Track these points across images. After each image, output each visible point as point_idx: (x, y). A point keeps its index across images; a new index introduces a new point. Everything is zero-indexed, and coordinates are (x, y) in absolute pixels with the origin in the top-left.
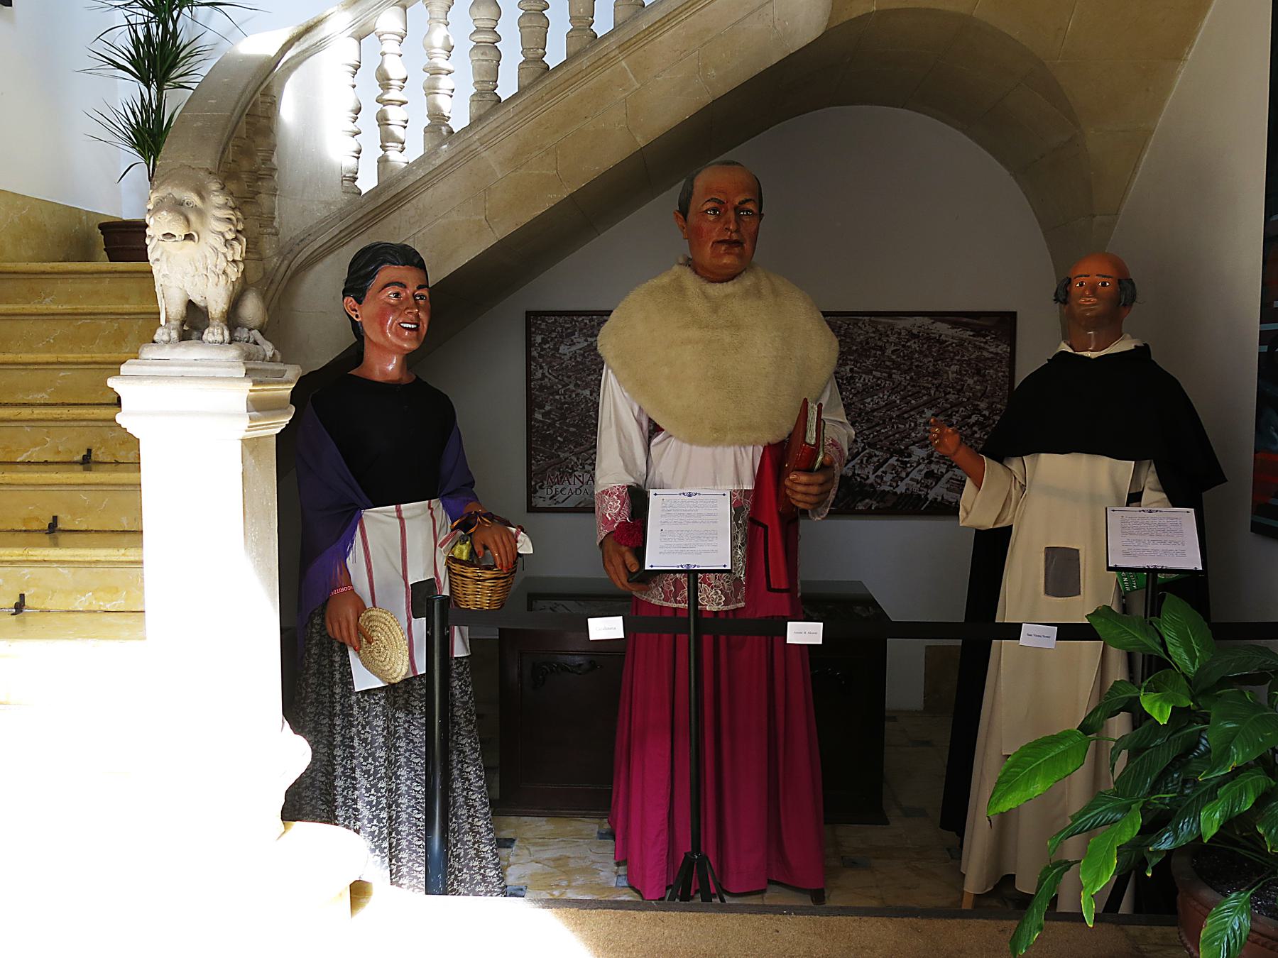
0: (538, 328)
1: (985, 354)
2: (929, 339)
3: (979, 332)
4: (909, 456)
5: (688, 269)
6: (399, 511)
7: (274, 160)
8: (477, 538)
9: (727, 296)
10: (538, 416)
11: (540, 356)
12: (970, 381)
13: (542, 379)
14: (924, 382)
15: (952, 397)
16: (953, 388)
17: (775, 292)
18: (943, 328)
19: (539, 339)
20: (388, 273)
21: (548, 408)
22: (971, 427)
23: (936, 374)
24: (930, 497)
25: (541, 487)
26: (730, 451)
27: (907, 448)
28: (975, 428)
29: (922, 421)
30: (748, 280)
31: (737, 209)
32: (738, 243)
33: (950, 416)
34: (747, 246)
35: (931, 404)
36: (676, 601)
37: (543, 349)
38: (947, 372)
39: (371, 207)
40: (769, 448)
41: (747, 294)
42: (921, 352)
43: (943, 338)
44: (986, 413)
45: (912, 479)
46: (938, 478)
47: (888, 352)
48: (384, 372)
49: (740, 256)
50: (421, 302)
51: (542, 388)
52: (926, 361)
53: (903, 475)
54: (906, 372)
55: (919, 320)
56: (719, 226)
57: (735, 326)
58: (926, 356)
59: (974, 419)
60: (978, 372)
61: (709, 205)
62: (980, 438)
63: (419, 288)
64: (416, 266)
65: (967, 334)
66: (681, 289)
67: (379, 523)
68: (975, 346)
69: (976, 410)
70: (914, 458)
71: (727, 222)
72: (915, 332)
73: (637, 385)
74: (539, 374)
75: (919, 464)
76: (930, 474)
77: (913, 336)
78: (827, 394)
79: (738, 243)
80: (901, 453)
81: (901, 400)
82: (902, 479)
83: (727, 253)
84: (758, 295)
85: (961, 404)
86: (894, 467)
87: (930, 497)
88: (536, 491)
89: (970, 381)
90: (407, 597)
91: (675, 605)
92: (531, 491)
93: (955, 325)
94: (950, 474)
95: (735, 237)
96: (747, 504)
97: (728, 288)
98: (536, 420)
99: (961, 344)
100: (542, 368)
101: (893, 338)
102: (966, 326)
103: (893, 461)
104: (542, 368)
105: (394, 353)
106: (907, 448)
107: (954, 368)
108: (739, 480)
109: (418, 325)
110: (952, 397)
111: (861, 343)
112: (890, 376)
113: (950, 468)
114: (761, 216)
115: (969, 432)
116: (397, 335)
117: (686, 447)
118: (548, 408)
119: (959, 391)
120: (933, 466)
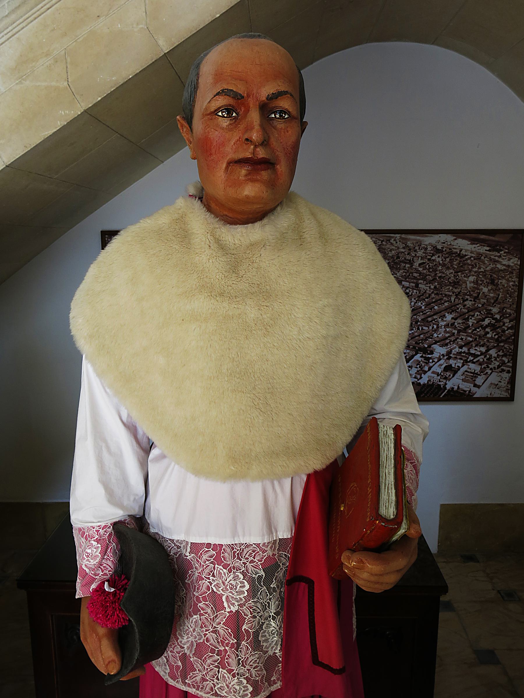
1: (499, 266)
2: (451, 253)
3: (494, 247)
4: (432, 353)
5: (197, 204)
9: (252, 245)
12: (485, 290)
14: (445, 290)
15: (469, 304)
16: (470, 295)
17: (323, 237)
18: (463, 244)
22: (484, 328)
23: (456, 284)
24: (448, 387)
26: (256, 489)
27: (429, 346)
28: (488, 330)
29: (443, 323)
30: (284, 220)
31: (265, 108)
32: (267, 164)
33: (467, 319)
34: (282, 168)
35: (451, 309)
36: (185, 683)
38: (465, 282)
40: (315, 480)
41: (281, 242)
42: (444, 265)
43: (463, 252)
44: (498, 316)
45: (433, 372)
46: (455, 371)
47: (416, 264)
49: (271, 184)
52: (448, 272)
53: (426, 368)
54: (431, 282)
55: (443, 237)
56: (235, 136)
57: (263, 293)
58: (448, 268)
59: (487, 321)
60: (492, 282)
61: (221, 101)
62: (492, 338)
65: (483, 249)
66: (184, 236)
68: (491, 259)
69: (489, 314)
70: (436, 355)
71: (249, 128)
72: (439, 247)
73: (124, 382)
75: (439, 359)
76: (448, 368)
77: (437, 251)
78: (395, 377)
79: (267, 164)
80: (425, 351)
81: (426, 306)
82: (425, 372)
83: (250, 178)
84: (300, 241)
85: (476, 309)
86: (418, 363)
87: (448, 387)
89: (485, 290)
91: (184, 688)
93: (473, 241)
94: (465, 368)
95: (261, 153)
96: (284, 563)
97: (254, 232)
99: (479, 257)
101: (420, 253)
102: (482, 242)
103: (418, 357)
106: (429, 346)
107: (472, 279)
108: (270, 525)
110: (469, 304)
111: (392, 257)
112: (417, 285)
113: (466, 362)
114: (303, 126)
115: (482, 333)
117: (192, 479)
119: (476, 298)
120: (452, 362)
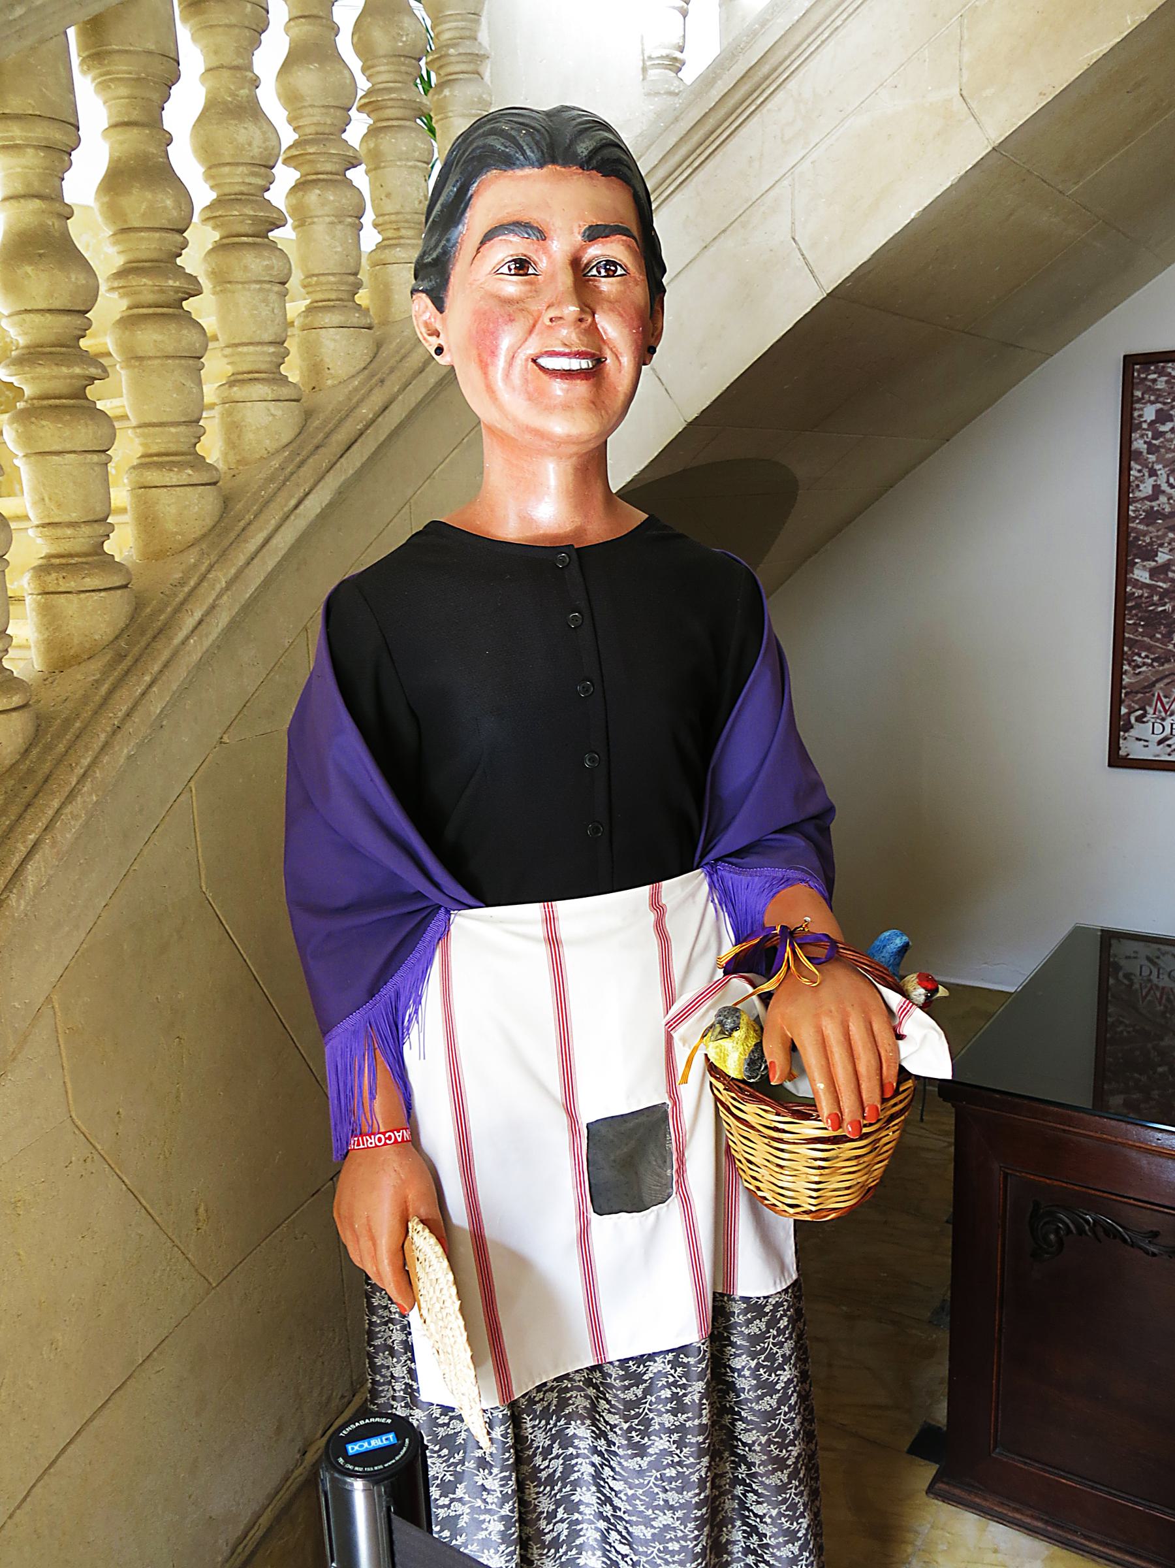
0: (1150, 390)
6: (550, 920)
7: (483, 36)
8: (779, 1016)
10: (1141, 574)
11: (1152, 449)
13: (1154, 497)
19: (1149, 413)
20: (497, 196)
21: (1162, 557)
25: (1139, 719)
37: (1158, 435)
39: (695, 114)
48: (526, 520)
50: (607, 285)
51: (1152, 516)
63: (594, 234)
64: (586, 164)
67: (489, 954)
74: (1146, 489)
88: (1128, 727)
90: (576, 1156)
92: (1118, 726)
98: (1137, 584)
100: (1153, 473)
104: (1153, 473)
105: (541, 452)
109: (599, 361)
116: (536, 397)
118: (1162, 557)
